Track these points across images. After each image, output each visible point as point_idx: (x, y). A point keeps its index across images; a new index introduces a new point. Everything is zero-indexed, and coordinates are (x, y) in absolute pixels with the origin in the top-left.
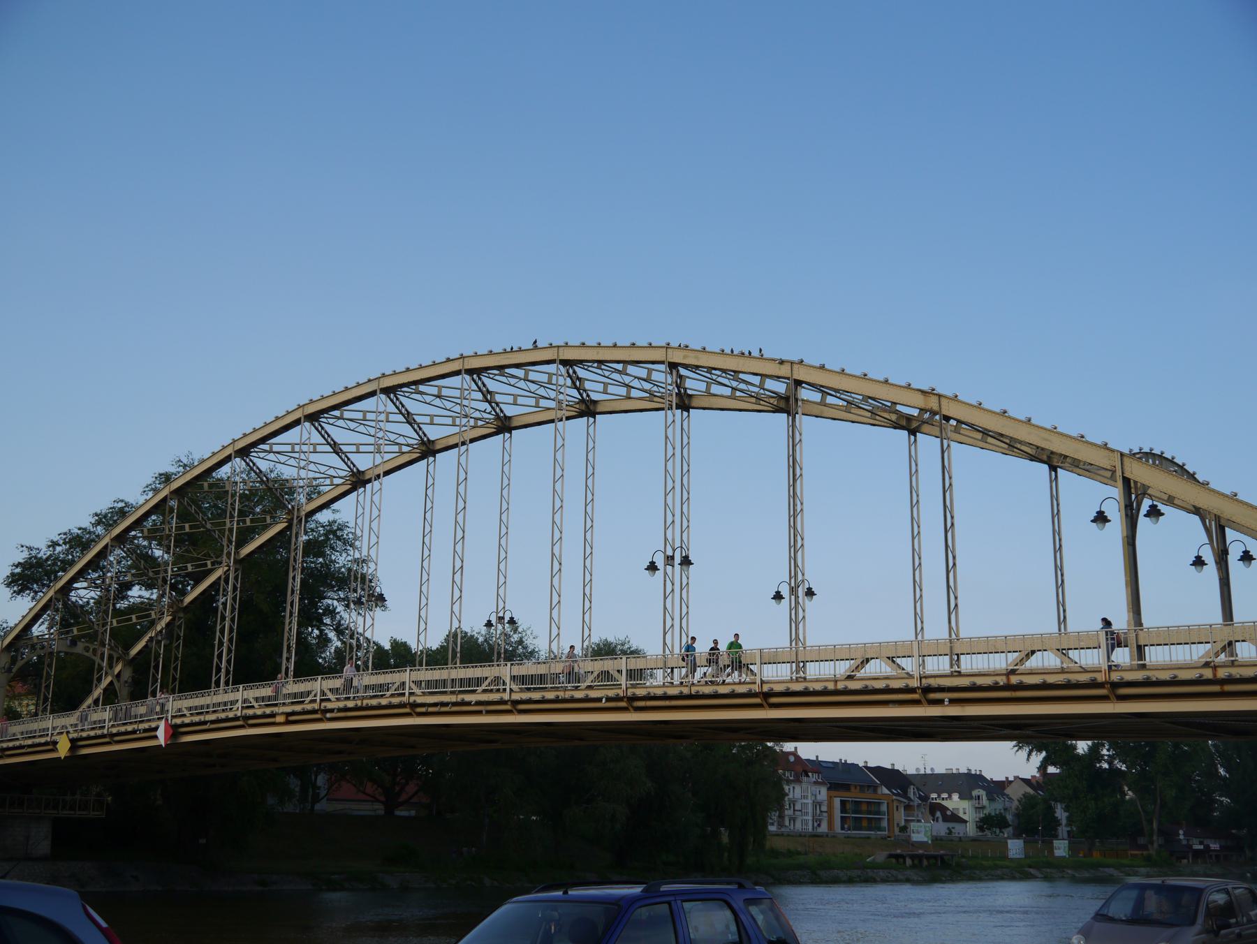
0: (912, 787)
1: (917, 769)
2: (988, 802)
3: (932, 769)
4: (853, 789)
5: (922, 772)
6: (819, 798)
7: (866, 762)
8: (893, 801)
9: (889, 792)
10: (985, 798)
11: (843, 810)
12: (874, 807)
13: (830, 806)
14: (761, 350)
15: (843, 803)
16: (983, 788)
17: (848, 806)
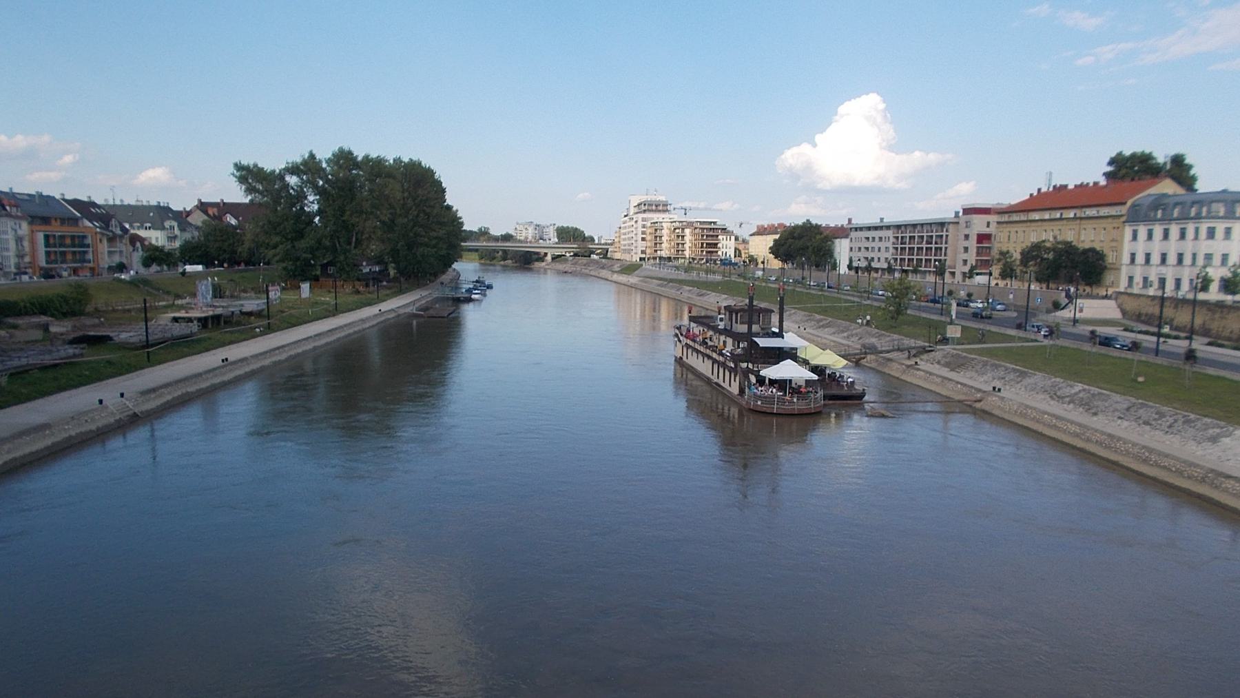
0: (113, 220)
1: (106, 200)
2: (179, 232)
3: (122, 201)
4: (53, 221)
5: (111, 203)
6: (20, 232)
7: (63, 195)
8: (96, 233)
9: (91, 225)
10: (176, 228)
11: (47, 245)
12: (79, 241)
13: (33, 242)
14: (848, 114)
15: (47, 237)
16: (175, 219)
17: (52, 241)
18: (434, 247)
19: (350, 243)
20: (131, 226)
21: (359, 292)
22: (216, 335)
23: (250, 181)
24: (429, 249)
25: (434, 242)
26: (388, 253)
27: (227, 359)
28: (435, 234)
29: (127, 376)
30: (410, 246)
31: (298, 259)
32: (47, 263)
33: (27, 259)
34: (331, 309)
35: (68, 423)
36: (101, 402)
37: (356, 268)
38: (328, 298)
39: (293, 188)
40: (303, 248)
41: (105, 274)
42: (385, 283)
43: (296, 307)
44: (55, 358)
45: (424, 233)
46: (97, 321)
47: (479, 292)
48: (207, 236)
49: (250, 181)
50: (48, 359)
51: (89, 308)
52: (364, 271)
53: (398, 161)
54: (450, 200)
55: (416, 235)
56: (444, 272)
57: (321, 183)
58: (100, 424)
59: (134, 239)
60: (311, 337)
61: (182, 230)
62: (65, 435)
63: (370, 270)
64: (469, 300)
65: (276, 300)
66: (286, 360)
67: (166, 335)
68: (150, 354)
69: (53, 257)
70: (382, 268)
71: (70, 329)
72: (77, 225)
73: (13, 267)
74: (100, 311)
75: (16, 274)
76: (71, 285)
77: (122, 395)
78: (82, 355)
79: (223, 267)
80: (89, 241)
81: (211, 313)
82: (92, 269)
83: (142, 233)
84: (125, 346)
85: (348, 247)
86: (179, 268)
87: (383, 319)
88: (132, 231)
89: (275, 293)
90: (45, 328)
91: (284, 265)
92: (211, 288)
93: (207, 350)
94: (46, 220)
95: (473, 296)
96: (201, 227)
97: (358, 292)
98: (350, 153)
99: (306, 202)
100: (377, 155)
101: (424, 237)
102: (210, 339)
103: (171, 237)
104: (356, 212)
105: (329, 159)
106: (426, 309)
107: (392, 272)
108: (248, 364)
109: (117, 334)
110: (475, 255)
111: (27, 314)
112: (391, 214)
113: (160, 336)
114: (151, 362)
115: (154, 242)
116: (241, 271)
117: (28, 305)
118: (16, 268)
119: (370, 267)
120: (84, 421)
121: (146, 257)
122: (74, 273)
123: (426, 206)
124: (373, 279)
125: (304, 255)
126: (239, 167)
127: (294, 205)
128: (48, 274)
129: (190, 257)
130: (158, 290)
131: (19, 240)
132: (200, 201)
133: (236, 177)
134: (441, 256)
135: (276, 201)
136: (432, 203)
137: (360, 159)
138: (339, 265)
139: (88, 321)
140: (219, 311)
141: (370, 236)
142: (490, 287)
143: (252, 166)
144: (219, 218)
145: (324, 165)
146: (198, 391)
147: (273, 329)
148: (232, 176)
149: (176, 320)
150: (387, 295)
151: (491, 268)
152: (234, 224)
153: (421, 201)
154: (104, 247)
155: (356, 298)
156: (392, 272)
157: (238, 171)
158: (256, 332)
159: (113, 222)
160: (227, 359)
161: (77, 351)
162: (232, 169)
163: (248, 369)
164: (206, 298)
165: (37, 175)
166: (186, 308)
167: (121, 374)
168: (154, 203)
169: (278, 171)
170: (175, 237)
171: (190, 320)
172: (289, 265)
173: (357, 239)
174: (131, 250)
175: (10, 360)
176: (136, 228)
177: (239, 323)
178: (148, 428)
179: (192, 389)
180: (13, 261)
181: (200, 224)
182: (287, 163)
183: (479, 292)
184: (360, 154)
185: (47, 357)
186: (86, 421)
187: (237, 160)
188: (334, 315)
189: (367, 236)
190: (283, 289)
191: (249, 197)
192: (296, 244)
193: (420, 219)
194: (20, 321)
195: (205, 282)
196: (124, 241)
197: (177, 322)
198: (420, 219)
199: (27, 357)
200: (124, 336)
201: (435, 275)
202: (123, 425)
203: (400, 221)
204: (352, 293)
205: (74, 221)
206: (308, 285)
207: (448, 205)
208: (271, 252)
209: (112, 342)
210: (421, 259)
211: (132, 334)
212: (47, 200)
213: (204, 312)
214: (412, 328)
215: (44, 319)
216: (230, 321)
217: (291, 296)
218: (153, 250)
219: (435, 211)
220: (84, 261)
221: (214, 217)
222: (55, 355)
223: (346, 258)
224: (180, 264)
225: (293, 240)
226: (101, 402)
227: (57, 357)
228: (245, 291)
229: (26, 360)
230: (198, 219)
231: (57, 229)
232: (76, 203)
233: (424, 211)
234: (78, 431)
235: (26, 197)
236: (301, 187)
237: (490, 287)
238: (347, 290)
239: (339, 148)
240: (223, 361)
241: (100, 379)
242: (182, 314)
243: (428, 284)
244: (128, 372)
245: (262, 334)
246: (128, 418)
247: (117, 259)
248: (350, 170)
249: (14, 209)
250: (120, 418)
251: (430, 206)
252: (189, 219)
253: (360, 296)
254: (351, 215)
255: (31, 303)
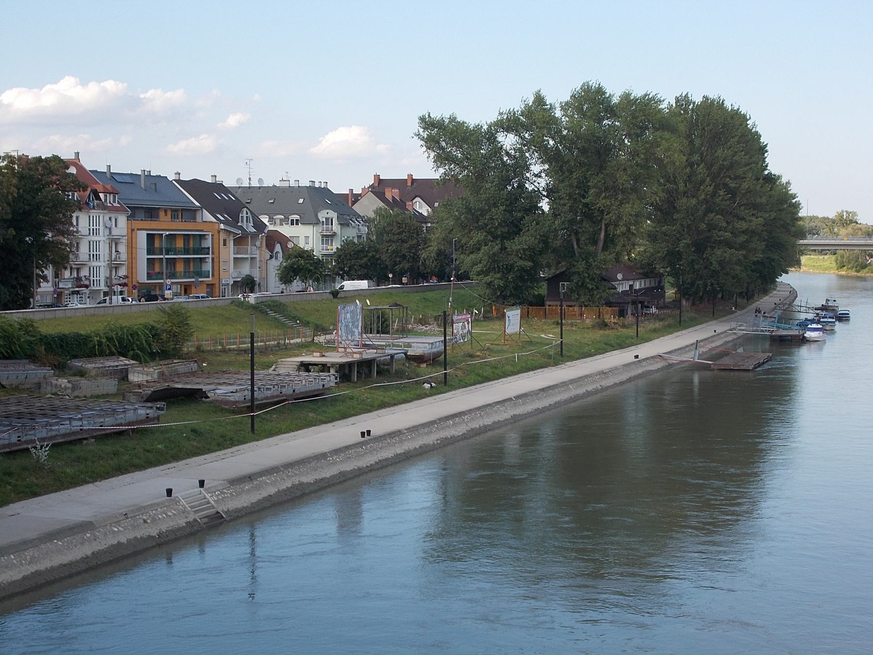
2: (339, 227)
3: (260, 180)
4: (162, 214)
6: (115, 232)
11: (150, 251)
15: (151, 238)
18: (742, 246)
19: (595, 242)
20: (271, 219)
21: (606, 325)
22: (361, 392)
23: (444, 144)
24: (733, 250)
25: (742, 238)
26: (663, 259)
27: (369, 432)
28: (744, 225)
29: (218, 453)
30: (700, 247)
31: (509, 268)
32: (147, 280)
33: (123, 272)
34: (552, 353)
35: (118, 523)
36: (169, 492)
37: (604, 283)
38: (549, 335)
39: (508, 154)
40: (518, 251)
41: (229, 296)
42: (654, 310)
43: (496, 348)
44: (119, 422)
45: (725, 225)
46: (194, 366)
47: (820, 326)
48: (382, 234)
49: (444, 144)
50: (109, 423)
51: (188, 347)
52: (620, 289)
53: (683, 102)
54: (774, 164)
55: (711, 227)
56: (765, 292)
57: (551, 142)
58: (164, 528)
59: (273, 239)
60: (510, 399)
61: (344, 224)
62: (112, 541)
63: (631, 286)
64: (803, 341)
65: (463, 337)
66: (464, 437)
67: (284, 390)
68: (256, 420)
69: (157, 269)
70: (653, 285)
71: (156, 376)
72: (194, 218)
73: (103, 283)
74: (203, 351)
75: (106, 294)
76: (164, 311)
77: (202, 483)
78: (158, 418)
79: (402, 283)
80: (208, 243)
81: (357, 357)
82: (211, 286)
83: (286, 230)
84: (223, 407)
85: (592, 248)
86: (336, 284)
87: (640, 371)
88: (271, 228)
89: (461, 326)
90: (123, 375)
91: (488, 279)
92: (360, 317)
93: (344, 416)
94: (151, 213)
95: (808, 334)
96: (374, 220)
97: (604, 325)
98: (600, 91)
99: (528, 175)
100: (643, 93)
101: (726, 231)
102: (352, 398)
103: (327, 236)
104: (607, 189)
105: (567, 103)
106: (716, 357)
107: (670, 292)
108: (401, 441)
109: (212, 387)
110: (828, 261)
111: (102, 354)
112: (668, 192)
113: (274, 392)
114: (255, 433)
115: (302, 244)
116: (431, 289)
117: (104, 340)
118: (106, 285)
119: (631, 283)
120: (142, 521)
121: (285, 267)
122: (186, 293)
123: (729, 177)
124: (634, 303)
125: (520, 263)
126: (427, 123)
127: (509, 181)
128: (149, 294)
129: (350, 268)
130: (294, 318)
131: (114, 242)
132: (377, 177)
133: (423, 139)
134: (754, 263)
135: (480, 176)
136: (740, 172)
137: (615, 100)
138: (575, 278)
139: (180, 366)
140: (370, 354)
141: (629, 230)
142: (843, 318)
143: (447, 121)
144: (399, 204)
145: (558, 113)
146: (317, 482)
147: (451, 385)
148: (416, 138)
149: (306, 367)
150: (655, 331)
151: (860, 284)
152: (425, 214)
153: (721, 169)
154: (229, 252)
155: (598, 334)
156: (670, 292)
157: (425, 129)
158: (424, 388)
159: (244, 213)
160: (369, 432)
161: (152, 413)
162: (415, 126)
163: (399, 449)
164: (353, 333)
165: (182, 144)
166: (323, 349)
167: (210, 451)
168: (305, 183)
169: (485, 127)
170: (334, 235)
171: (324, 368)
172: (495, 278)
173: (607, 235)
174: (268, 257)
175: (57, 424)
176: (278, 222)
177: (400, 375)
178: (244, 537)
179: (308, 478)
180: (103, 274)
181: (372, 215)
182: (501, 114)
183: (820, 326)
184: (615, 91)
185: (109, 420)
186: (145, 521)
187: (423, 112)
188: (556, 364)
189: (624, 229)
190: (476, 321)
191: (442, 171)
192: (507, 244)
193: (718, 200)
194: (90, 365)
195: (352, 307)
196: (258, 243)
197: (308, 371)
198: (718, 200)
199: (80, 419)
200: (222, 390)
201: (749, 296)
202: (198, 531)
203: (683, 202)
204: (593, 327)
205: (190, 213)
206: (519, 312)
207: (770, 174)
208: (469, 259)
209: (208, 400)
210: (718, 268)
211: (233, 388)
212: (156, 182)
213: (346, 354)
214: (692, 390)
215: (123, 361)
216: (388, 371)
217: (488, 331)
218: (296, 257)
219: (745, 185)
220: (200, 274)
221: (393, 203)
222: (121, 418)
223: (589, 266)
224: (338, 278)
225: (505, 237)
226: (169, 492)
227: (123, 422)
228: (423, 322)
229: (80, 423)
230: (369, 207)
231: (165, 225)
232: (194, 186)
233: (725, 185)
234: (131, 536)
235: (129, 180)
236: (520, 150)
237: (843, 318)
238: (588, 321)
239: (584, 85)
240: (363, 434)
241: (177, 458)
242: (315, 358)
243: (733, 312)
244: (221, 446)
245: (433, 392)
246: (206, 520)
247: (246, 270)
248: (600, 121)
249: (110, 198)
250: (195, 520)
251: (736, 178)
252: (357, 208)
253: (607, 332)
254: (598, 195)
255: (107, 338)
